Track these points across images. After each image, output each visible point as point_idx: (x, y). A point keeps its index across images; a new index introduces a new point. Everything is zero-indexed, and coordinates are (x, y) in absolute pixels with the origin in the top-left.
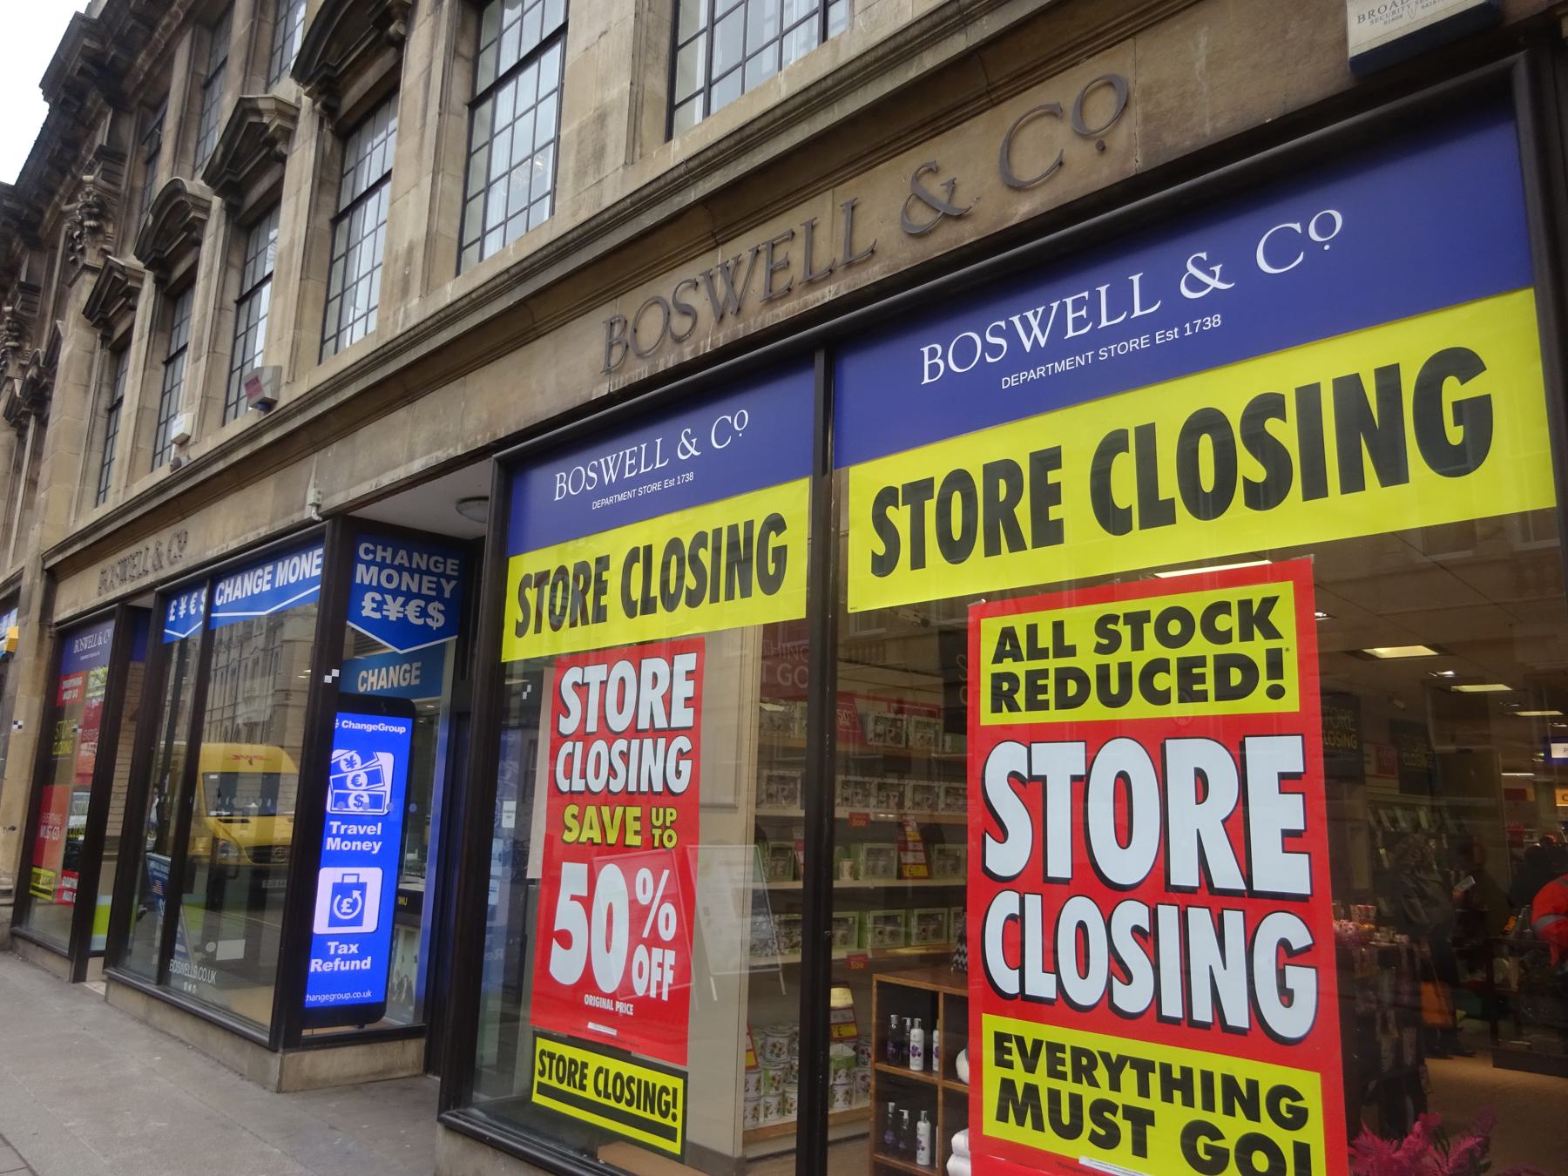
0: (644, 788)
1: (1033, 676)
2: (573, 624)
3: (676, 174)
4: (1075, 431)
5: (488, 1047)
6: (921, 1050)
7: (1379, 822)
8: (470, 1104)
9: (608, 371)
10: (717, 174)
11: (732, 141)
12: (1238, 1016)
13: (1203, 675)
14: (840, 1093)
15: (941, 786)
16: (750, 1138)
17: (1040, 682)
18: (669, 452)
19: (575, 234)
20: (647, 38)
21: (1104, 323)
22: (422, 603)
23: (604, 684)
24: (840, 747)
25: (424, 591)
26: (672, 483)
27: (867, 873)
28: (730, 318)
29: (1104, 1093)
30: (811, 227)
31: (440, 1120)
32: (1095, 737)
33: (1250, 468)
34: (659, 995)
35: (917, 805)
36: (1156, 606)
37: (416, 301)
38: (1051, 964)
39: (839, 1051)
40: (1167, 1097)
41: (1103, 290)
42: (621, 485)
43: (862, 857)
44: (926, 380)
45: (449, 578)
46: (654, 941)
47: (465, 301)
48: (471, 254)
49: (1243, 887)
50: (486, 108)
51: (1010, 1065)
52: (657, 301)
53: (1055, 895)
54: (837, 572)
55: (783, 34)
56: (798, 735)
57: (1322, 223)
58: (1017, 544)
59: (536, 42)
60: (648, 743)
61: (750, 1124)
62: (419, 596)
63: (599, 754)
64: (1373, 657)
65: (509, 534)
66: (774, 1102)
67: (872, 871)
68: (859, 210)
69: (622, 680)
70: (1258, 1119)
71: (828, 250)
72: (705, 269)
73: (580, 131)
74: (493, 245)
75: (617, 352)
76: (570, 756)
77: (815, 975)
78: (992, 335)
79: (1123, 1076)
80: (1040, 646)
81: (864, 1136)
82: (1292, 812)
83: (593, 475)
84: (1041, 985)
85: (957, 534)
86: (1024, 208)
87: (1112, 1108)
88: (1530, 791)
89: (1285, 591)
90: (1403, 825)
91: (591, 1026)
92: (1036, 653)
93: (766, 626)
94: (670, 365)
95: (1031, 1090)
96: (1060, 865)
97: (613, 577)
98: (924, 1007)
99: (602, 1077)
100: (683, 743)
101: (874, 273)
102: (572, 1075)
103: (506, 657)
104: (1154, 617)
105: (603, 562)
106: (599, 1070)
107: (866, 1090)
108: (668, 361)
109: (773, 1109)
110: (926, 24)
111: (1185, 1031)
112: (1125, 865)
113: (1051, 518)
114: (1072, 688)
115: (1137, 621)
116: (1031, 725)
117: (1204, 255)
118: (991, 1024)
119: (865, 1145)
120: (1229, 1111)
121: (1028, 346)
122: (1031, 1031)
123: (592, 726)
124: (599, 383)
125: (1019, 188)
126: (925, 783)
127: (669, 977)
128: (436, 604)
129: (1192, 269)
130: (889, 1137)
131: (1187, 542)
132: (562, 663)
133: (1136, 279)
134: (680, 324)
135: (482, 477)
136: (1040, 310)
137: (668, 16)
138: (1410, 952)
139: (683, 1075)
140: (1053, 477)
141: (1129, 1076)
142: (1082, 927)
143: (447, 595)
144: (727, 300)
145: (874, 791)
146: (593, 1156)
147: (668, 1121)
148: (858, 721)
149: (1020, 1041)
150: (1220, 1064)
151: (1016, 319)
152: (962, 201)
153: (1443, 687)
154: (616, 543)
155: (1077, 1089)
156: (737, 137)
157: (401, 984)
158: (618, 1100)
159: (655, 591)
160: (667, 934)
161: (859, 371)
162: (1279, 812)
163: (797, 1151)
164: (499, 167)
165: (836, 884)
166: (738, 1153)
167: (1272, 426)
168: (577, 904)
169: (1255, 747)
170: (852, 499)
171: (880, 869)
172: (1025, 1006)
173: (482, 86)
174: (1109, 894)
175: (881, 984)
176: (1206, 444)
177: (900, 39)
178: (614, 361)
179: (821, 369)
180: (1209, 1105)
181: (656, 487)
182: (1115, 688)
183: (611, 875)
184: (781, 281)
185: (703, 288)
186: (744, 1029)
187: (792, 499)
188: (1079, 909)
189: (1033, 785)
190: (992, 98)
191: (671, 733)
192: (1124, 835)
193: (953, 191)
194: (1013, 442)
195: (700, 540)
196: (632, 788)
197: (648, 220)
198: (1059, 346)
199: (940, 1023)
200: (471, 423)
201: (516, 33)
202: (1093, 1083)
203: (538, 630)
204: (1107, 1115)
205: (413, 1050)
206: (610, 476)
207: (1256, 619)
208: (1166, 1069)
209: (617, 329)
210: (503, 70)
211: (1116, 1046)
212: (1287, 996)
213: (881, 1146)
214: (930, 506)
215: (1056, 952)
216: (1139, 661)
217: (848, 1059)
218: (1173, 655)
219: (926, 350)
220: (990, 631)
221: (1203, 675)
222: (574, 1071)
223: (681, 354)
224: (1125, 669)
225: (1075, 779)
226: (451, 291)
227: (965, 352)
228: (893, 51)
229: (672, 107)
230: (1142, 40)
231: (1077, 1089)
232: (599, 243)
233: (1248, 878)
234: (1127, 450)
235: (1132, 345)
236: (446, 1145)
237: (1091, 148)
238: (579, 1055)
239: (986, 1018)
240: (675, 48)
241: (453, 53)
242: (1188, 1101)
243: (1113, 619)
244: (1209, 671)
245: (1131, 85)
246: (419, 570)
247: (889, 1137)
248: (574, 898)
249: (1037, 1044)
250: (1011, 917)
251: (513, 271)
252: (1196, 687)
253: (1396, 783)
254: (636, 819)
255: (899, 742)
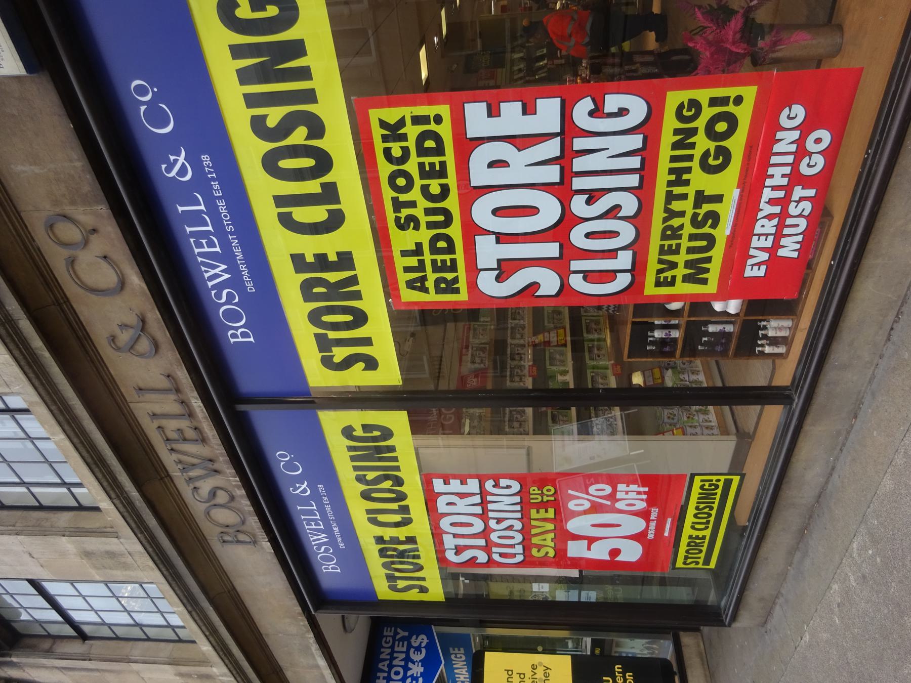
0: (518, 508)
1: (436, 269)
2: (418, 557)
3: (120, 506)
4: (279, 245)
5: (682, 595)
6: (667, 331)
7: (521, 78)
8: (719, 607)
9: (255, 542)
10: (119, 478)
11: (96, 470)
12: (636, 141)
13: (430, 164)
14: (694, 377)
15: (511, 323)
16: (725, 432)
17: (439, 264)
18: (306, 501)
19: (163, 569)
20: (33, 526)
21: (210, 228)
22: (412, 650)
23: (455, 536)
24: (489, 386)
25: (404, 649)
26: (325, 498)
27: (564, 365)
28: (216, 466)
29: (686, 220)
30: (154, 415)
31: (730, 625)
32: (472, 230)
33: (299, 136)
34: (645, 493)
35: (522, 337)
36: (388, 194)
37: (215, 670)
38: (611, 254)
39: (670, 380)
40: (687, 183)
41: (188, 229)
42: (328, 531)
43: (555, 368)
44: (252, 339)
45: (396, 633)
46: (612, 497)
47: (211, 639)
48: (183, 634)
49: (559, 138)
50: (86, 629)
51: (674, 278)
52: (208, 513)
53: (569, 252)
54: (376, 392)
55: (29, 437)
56: (485, 411)
57: (140, 93)
58: (354, 280)
59: (40, 598)
60: (490, 507)
61: (716, 431)
62: (407, 653)
63: (499, 537)
64: (428, 80)
65: (361, 600)
66: (702, 417)
67: (563, 362)
68: (142, 385)
69: (452, 524)
70: (697, 128)
71: (170, 405)
72: (185, 484)
73: (96, 568)
74: (175, 620)
75: (242, 537)
76: (501, 555)
77: (626, 397)
78: (221, 299)
79: (676, 210)
80: (417, 265)
81: (717, 362)
82: (511, 110)
83: (323, 548)
84: (625, 260)
85: (349, 318)
86: (135, 280)
87: (695, 215)
88: (502, 3)
89: (375, 115)
90: (522, 66)
91: (666, 534)
92: (421, 266)
93: (414, 432)
94: (248, 503)
95: (688, 264)
96: (551, 250)
97: (388, 533)
98: (642, 330)
99: (697, 526)
100: (489, 485)
101: (183, 375)
102: (697, 545)
103: (441, 598)
104: (395, 195)
105: (380, 540)
106: (693, 528)
107: (690, 362)
108: (245, 504)
109: (706, 417)
110: (12, 346)
111: (647, 172)
112: (549, 211)
113: (336, 259)
114: (442, 244)
115: (398, 205)
116: (467, 271)
117: (164, 166)
118: (650, 289)
119: (722, 362)
120: (692, 146)
121: (227, 276)
122: (653, 266)
123: (482, 542)
124: (263, 548)
125: (122, 284)
126: (509, 331)
127: (634, 487)
128: (413, 640)
129: (173, 174)
130: (719, 348)
131: (346, 173)
132: (442, 560)
133: (180, 209)
134: (222, 498)
135: (329, 620)
136: (203, 269)
137: (19, 513)
138: (592, 58)
139: (693, 476)
140: (310, 259)
141: (676, 206)
142: (588, 235)
143: (406, 634)
144: (205, 468)
145: (515, 363)
146: (744, 528)
147: (721, 484)
148: (477, 373)
149: (659, 272)
150: (665, 152)
151: (210, 284)
152: (133, 320)
153: (444, 43)
154: (366, 533)
155: (685, 237)
156: (93, 466)
157: (648, 648)
158: (710, 515)
159: (395, 506)
160: (608, 489)
161: (248, 380)
162: (512, 117)
163: (730, 405)
164: (124, 619)
165: (572, 386)
166: (734, 438)
167: (271, 123)
168: (593, 546)
169: (472, 132)
170: (330, 385)
171: (562, 358)
172: (637, 269)
173: (71, 632)
174: (567, 221)
175: (629, 357)
176: (286, 164)
177: (23, 363)
178: (248, 539)
179: (243, 405)
180: (690, 158)
181: (328, 508)
182: (441, 218)
183: (573, 526)
184: (190, 434)
185: (197, 484)
186: (660, 437)
187: (332, 422)
188: (577, 236)
189: (504, 267)
190: (63, 302)
191: (483, 493)
192: (531, 211)
193: (125, 326)
194: (288, 284)
195: (360, 479)
196: (519, 515)
197: (152, 522)
198: (226, 256)
199: (650, 320)
200: (293, 629)
201: (32, 610)
202: (681, 227)
203: (423, 579)
204: (700, 218)
205: (687, 640)
206: (323, 538)
207: (394, 132)
208: (670, 184)
209: (227, 538)
210: (60, 619)
211: (658, 214)
212: (623, 112)
213: (724, 353)
214: (332, 335)
215: (603, 251)
216: (423, 203)
217: (674, 373)
218: (418, 183)
219: (232, 340)
220: (409, 296)
221: (430, 164)
222: (694, 543)
223: (241, 496)
224: (428, 212)
225: (498, 241)
226: (205, 647)
227: (233, 316)
228: (31, 367)
229: (81, 508)
230: (21, 207)
231: (685, 237)
232: (169, 553)
233: (551, 136)
234: (291, 213)
235: (223, 210)
236: (745, 621)
237: (94, 238)
238: (684, 541)
239: (646, 293)
240: (41, 508)
241: (49, 653)
242: (688, 170)
243: (397, 219)
244: (427, 160)
245: (52, 213)
246: (391, 654)
247: (719, 348)
248: (589, 549)
249: (660, 261)
250: (585, 279)
251: (190, 608)
252: (438, 168)
253: (499, 70)
254: (538, 512)
255: (485, 348)
